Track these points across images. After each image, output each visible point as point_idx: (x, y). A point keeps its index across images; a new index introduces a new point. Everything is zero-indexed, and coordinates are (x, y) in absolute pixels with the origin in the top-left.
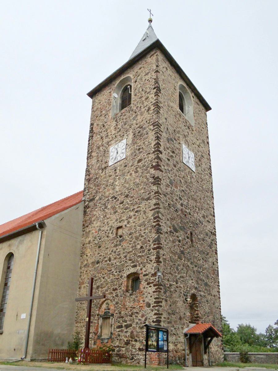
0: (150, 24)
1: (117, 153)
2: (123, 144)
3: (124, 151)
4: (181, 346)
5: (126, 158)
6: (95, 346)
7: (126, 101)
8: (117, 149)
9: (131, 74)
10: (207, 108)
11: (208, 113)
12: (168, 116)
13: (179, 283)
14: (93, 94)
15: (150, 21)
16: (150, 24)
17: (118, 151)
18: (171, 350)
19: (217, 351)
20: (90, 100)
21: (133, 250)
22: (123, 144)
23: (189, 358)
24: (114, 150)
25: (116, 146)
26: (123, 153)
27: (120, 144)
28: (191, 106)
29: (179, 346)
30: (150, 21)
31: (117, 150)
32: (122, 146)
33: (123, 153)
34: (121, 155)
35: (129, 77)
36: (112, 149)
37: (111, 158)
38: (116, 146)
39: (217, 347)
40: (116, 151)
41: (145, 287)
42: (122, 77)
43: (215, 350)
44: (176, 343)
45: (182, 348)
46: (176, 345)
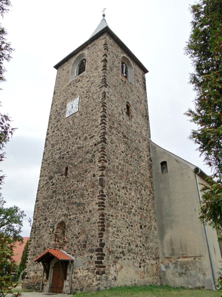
0: (104, 17)
1: (72, 107)
2: (76, 101)
3: (77, 106)
4: (40, 273)
5: (78, 111)
6: (171, 276)
7: (82, 69)
8: (72, 105)
9: (86, 52)
10: (145, 71)
11: (146, 75)
12: (115, 77)
13: (48, 219)
14: (57, 67)
15: (104, 16)
16: (104, 17)
17: (73, 106)
18: (31, 277)
19: (86, 276)
20: (55, 71)
21: (61, 188)
22: (76, 101)
23: (47, 284)
24: (70, 105)
25: (72, 103)
26: (76, 108)
27: (74, 101)
28: (133, 70)
29: (38, 273)
30: (104, 16)
31: (72, 106)
32: (76, 103)
33: (76, 108)
34: (75, 109)
35: (83, 53)
36: (69, 105)
37: (67, 111)
38: (72, 102)
39: (87, 271)
40: (71, 106)
41: (113, 216)
42: (80, 53)
43: (82, 275)
44: (36, 271)
45: (41, 274)
46: (36, 273)
